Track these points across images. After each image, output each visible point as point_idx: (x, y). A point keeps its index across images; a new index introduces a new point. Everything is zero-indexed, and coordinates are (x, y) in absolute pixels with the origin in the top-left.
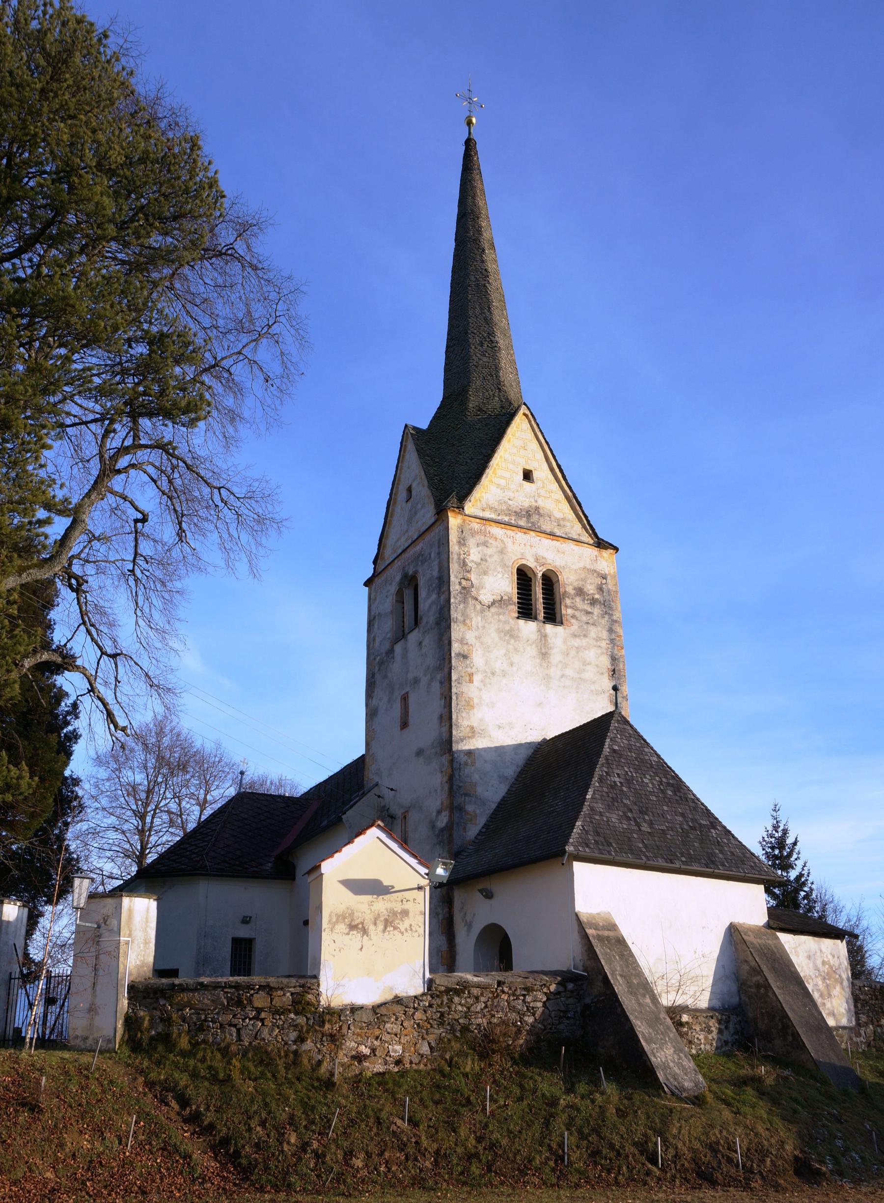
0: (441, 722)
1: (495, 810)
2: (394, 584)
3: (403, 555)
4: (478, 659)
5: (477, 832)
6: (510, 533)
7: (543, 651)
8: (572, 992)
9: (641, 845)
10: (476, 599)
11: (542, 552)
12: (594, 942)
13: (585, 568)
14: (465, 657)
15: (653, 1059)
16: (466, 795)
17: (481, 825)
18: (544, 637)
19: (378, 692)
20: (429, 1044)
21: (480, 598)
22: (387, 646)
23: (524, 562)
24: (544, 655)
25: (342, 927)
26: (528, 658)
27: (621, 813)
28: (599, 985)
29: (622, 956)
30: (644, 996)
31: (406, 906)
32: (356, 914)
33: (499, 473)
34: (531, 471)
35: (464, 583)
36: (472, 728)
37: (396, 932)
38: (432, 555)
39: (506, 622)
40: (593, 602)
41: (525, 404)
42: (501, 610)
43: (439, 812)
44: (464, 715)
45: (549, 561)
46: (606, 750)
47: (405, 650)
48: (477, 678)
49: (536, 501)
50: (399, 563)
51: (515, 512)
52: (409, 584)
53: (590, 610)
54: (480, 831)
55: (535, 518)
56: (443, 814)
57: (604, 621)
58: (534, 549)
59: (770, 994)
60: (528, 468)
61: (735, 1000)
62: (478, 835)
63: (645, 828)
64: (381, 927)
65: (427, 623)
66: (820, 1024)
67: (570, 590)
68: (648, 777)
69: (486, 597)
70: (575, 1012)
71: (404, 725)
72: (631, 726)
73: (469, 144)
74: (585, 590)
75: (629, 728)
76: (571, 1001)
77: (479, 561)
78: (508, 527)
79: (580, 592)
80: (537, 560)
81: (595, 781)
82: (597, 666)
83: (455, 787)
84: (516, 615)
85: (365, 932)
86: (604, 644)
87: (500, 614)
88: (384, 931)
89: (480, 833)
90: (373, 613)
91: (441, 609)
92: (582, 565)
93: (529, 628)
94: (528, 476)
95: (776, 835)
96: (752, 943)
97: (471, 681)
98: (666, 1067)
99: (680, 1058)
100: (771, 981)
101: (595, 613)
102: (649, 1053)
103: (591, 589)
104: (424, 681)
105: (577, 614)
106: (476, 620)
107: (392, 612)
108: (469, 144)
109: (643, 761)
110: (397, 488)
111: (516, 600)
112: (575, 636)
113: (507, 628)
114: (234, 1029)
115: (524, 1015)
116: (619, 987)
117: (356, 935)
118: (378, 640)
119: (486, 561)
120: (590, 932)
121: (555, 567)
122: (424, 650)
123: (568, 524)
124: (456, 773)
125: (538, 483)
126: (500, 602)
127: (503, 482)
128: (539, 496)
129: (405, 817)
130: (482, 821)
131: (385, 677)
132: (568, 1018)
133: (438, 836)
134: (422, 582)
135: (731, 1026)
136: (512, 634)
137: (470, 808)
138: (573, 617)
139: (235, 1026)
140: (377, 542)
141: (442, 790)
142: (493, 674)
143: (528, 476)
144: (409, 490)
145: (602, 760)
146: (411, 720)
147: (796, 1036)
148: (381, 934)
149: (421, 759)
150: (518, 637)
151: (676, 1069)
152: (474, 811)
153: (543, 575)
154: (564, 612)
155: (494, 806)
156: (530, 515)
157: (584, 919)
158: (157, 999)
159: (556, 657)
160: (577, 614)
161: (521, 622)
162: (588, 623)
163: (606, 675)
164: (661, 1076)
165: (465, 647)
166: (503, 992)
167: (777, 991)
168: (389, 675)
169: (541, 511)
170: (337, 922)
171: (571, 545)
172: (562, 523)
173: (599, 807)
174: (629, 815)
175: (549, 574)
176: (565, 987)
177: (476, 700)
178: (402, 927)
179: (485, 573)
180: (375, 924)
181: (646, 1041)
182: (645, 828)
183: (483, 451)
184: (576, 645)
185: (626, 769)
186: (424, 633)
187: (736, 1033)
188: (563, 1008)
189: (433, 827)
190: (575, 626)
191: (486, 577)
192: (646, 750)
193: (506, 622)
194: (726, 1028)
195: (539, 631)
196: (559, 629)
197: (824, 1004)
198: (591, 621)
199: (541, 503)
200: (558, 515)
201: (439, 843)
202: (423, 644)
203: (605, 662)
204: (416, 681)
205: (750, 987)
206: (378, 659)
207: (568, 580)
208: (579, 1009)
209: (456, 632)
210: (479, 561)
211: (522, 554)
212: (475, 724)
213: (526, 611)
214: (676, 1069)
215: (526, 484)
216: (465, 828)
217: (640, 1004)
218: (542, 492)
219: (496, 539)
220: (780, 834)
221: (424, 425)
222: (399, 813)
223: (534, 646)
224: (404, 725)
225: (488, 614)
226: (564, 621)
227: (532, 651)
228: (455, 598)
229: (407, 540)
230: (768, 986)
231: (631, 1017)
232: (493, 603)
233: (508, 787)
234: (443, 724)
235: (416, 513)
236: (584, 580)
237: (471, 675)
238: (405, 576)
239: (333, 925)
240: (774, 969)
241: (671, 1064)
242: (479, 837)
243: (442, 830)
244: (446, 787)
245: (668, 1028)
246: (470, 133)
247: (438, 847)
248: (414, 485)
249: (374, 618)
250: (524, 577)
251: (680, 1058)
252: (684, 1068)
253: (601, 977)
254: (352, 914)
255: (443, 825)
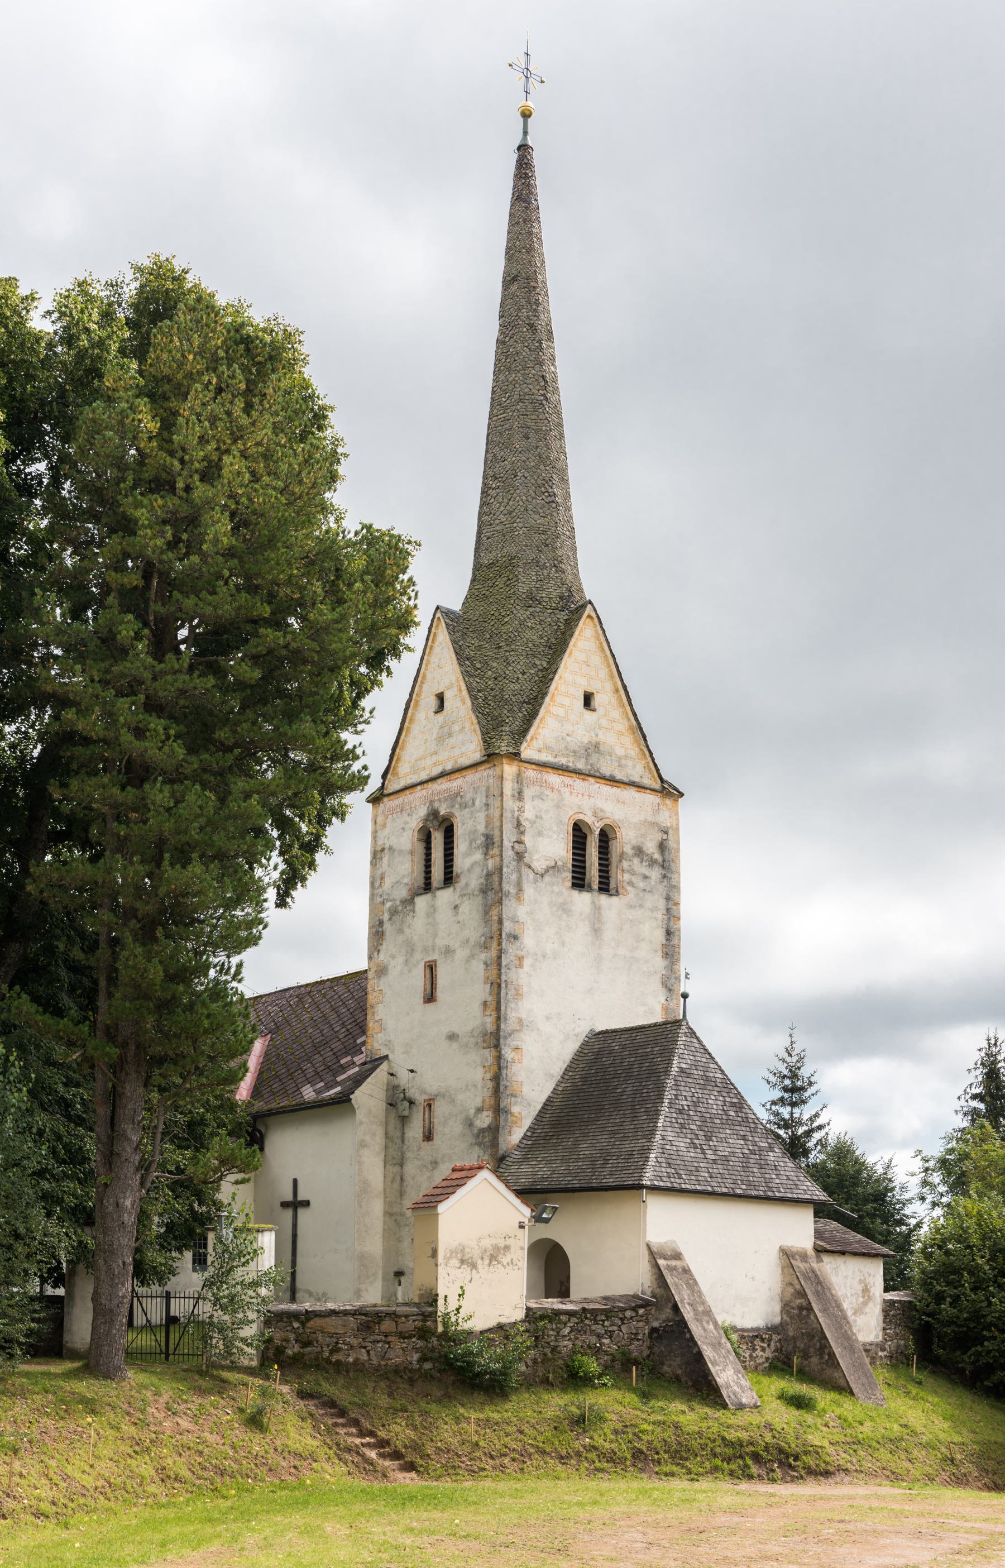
0: (484, 1010)
1: (540, 1111)
2: (415, 817)
3: (430, 785)
4: (529, 940)
5: (522, 1135)
6: (568, 780)
7: (597, 926)
8: (641, 1316)
9: (706, 1175)
10: (530, 867)
11: (600, 804)
12: (665, 1272)
13: (645, 821)
14: (516, 938)
15: (718, 1379)
16: (512, 1095)
17: (526, 1127)
18: (597, 909)
19: (389, 946)
20: (526, 1363)
21: (532, 866)
22: (403, 893)
23: (581, 817)
24: (596, 931)
25: (455, 1262)
26: (580, 934)
27: (688, 1141)
28: (668, 1312)
29: (688, 1284)
30: (708, 1323)
31: (508, 1242)
32: (467, 1250)
33: (559, 699)
34: (593, 694)
35: (517, 846)
36: (520, 1020)
37: (499, 1266)
38: (477, 803)
39: (560, 893)
40: (652, 862)
41: (590, 602)
42: (555, 879)
43: (479, 1110)
44: (513, 1005)
45: (608, 815)
46: (675, 1069)
47: (433, 910)
48: (527, 962)
49: (597, 735)
50: (424, 792)
51: (574, 752)
52: (439, 826)
53: (647, 874)
54: (525, 1135)
55: (594, 759)
56: (485, 1113)
57: (661, 889)
58: (592, 800)
59: (812, 1317)
60: (590, 690)
61: (777, 1320)
62: (523, 1138)
63: (711, 1156)
64: (487, 1262)
65: (467, 885)
66: (848, 1338)
67: (628, 850)
68: (713, 1097)
69: (539, 865)
70: (644, 1334)
71: (430, 998)
72: (698, 1038)
73: (523, 148)
74: (644, 849)
75: (695, 1041)
76: (641, 1324)
77: (534, 818)
78: (566, 774)
79: (639, 851)
80: (595, 815)
81: (665, 1108)
82: (651, 942)
83: (502, 1088)
84: (570, 884)
85: (474, 1266)
86: (660, 916)
87: (553, 884)
88: (490, 1264)
89: (525, 1137)
90: (380, 842)
91: (489, 875)
92: (642, 818)
93: (583, 900)
94: (588, 700)
95: (789, 1059)
96: (799, 1267)
97: (521, 966)
98: (728, 1386)
99: (739, 1378)
100: (814, 1305)
101: (653, 877)
102: (714, 1374)
103: (651, 847)
104: (461, 954)
105: (634, 879)
106: (529, 891)
107: (412, 853)
108: (523, 148)
109: (707, 1079)
110: (421, 687)
111: (570, 866)
112: (631, 907)
113: (561, 900)
114: (363, 1350)
115: (602, 1337)
116: (688, 1314)
117: (466, 1270)
118: (388, 883)
119: (541, 818)
120: (661, 1262)
121: (614, 821)
122: (460, 918)
123: (630, 763)
124: (504, 1072)
125: (600, 711)
126: (554, 868)
127: (561, 712)
128: (600, 728)
129: (430, 1106)
130: (527, 1122)
131: (400, 931)
132: (638, 1340)
133: (477, 1136)
134: (459, 831)
135: (773, 1344)
136: (565, 908)
137: (515, 1109)
138: (631, 883)
139: (365, 1348)
140: (390, 752)
141: (483, 1087)
142: (544, 956)
143: (588, 700)
144: (441, 698)
145: (670, 1082)
146: (439, 994)
147: (832, 1355)
148: (487, 1268)
149: (455, 1045)
150: (570, 910)
151: (735, 1388)
152: (520, 1113)
153: (602, 830)
154: (620, 877)
155: (539, 1107)
156: (588, 755)
157: (655, 1249)
158: (291, 1322)
159: (609, 932)
160: (634, 879)
161: (575, 893)
162: (645, 890)
163: (660, 954)
164: (724, 1393)
165: (517, 926)
166: (586, 1318)
167: (819, 1314)
168: (407, 931)
169: (601, 748)
170: (451, 1257)
171: (631, 793)
172: (623, 762)
173: (670, 1135)
174: (696, 1141)
175: (605, 829)
176: (637, 1313)
177: (525, 989)
178: (505, 1260)
179: (540, 834)
180: (482, 1259)
181: (712, 1363)
182: (711, 1156)
183: (538, 662)
184: (631, 917)
185: (693, 1090)
186: (462, 896)
187: (776, 1350)
188: (634, 1331)
189: (471, 1125)
190: (631, 895)
191: (540, 839)
192: (712, 1066)
193: (560, 893)
194: (769, 1345)
195: (593, 902)
196: (614, 900)
197: (855, 1321)
198: (648, 889)
199: (601, 737)
200: (620, 751)
201: (479, 1144)
202: (461, 910)
203: (660, 936)
204: (448, 951)
205: (793, 1308)
206: (388, 904)
207: (625, 840)
208: (646, 1332)
209: (510, 907)
210: (534, 818)
211: (579, 807)
212: (523, 1016)
213: (579, 882)
214: (735, 1388)
215: (587, 714)
216: (510, 1132)
217: (705, 1330)
218: (604, 722)
219: (553, 789)
220: (795, 1059)
221: (456, 605)
222: (420, 1098)
223: (587, 923)
224: (430, 998)
225: (541, 884)
226: (620, 890)
227: (583, 928)
228: (508, 867)
229: (435, 764)
230: (809, 1309)
231: (699, 1343)
232: (547, 871)
233: (553, 1086)
234: (488, 1013)
235: (450, 735)
236: (643, 836)
237: (521, 959)
238: (434, 814)
239: (447, 1259)
240: (817, 1293)
241: (732, 1384)
242: (525, 1142)
243: (482, 1131)
244: (490, 1085)
245: (729, 1352)
246: (525, 133)
247: (476, 1148)
248: (447, 696)
249: (383, 850)
250: (579, 833)
251: (739, 1378)
252: (741, 1387)
253: (670, 1305)
254: (463, 1251)
255: (485, 1125)
